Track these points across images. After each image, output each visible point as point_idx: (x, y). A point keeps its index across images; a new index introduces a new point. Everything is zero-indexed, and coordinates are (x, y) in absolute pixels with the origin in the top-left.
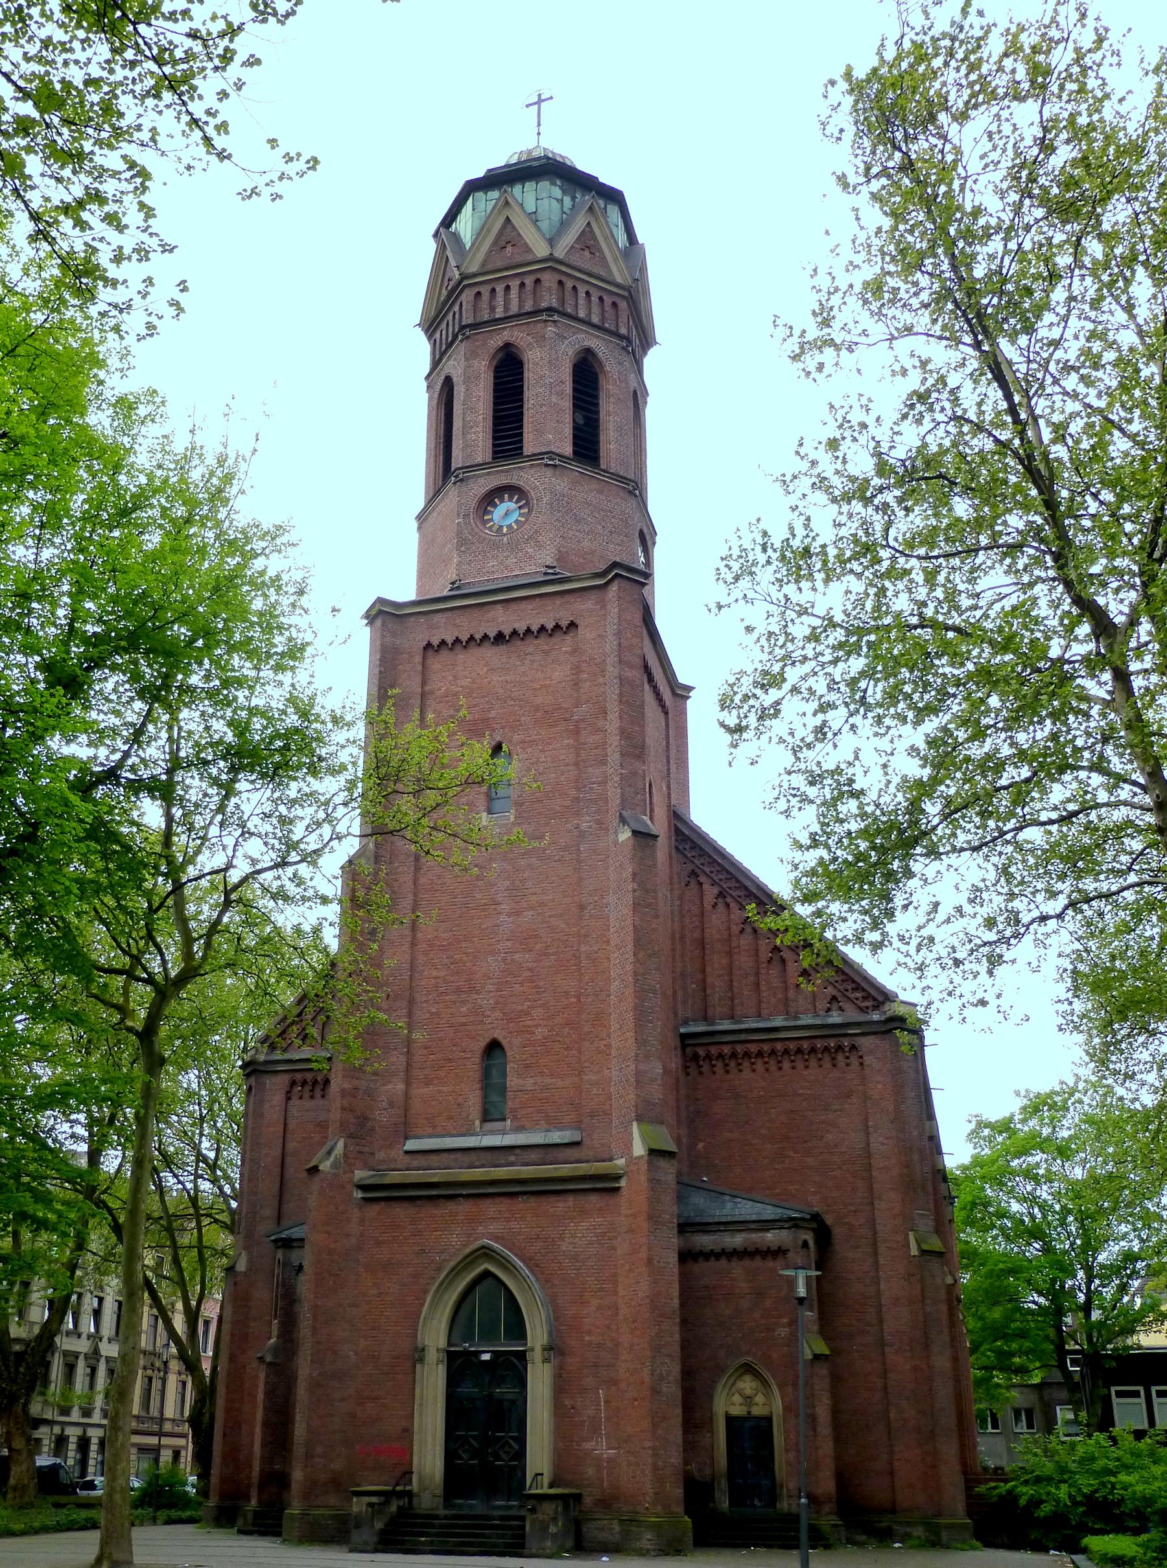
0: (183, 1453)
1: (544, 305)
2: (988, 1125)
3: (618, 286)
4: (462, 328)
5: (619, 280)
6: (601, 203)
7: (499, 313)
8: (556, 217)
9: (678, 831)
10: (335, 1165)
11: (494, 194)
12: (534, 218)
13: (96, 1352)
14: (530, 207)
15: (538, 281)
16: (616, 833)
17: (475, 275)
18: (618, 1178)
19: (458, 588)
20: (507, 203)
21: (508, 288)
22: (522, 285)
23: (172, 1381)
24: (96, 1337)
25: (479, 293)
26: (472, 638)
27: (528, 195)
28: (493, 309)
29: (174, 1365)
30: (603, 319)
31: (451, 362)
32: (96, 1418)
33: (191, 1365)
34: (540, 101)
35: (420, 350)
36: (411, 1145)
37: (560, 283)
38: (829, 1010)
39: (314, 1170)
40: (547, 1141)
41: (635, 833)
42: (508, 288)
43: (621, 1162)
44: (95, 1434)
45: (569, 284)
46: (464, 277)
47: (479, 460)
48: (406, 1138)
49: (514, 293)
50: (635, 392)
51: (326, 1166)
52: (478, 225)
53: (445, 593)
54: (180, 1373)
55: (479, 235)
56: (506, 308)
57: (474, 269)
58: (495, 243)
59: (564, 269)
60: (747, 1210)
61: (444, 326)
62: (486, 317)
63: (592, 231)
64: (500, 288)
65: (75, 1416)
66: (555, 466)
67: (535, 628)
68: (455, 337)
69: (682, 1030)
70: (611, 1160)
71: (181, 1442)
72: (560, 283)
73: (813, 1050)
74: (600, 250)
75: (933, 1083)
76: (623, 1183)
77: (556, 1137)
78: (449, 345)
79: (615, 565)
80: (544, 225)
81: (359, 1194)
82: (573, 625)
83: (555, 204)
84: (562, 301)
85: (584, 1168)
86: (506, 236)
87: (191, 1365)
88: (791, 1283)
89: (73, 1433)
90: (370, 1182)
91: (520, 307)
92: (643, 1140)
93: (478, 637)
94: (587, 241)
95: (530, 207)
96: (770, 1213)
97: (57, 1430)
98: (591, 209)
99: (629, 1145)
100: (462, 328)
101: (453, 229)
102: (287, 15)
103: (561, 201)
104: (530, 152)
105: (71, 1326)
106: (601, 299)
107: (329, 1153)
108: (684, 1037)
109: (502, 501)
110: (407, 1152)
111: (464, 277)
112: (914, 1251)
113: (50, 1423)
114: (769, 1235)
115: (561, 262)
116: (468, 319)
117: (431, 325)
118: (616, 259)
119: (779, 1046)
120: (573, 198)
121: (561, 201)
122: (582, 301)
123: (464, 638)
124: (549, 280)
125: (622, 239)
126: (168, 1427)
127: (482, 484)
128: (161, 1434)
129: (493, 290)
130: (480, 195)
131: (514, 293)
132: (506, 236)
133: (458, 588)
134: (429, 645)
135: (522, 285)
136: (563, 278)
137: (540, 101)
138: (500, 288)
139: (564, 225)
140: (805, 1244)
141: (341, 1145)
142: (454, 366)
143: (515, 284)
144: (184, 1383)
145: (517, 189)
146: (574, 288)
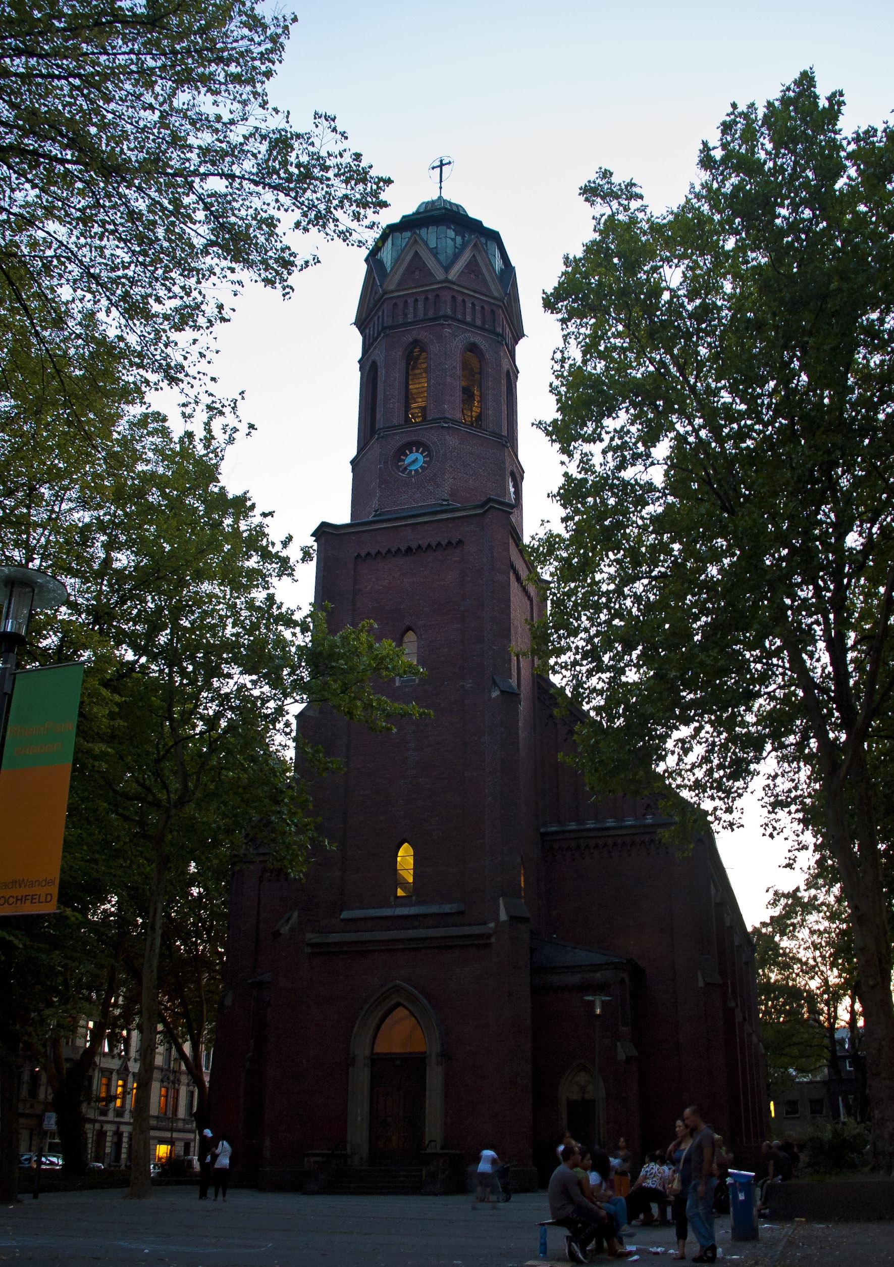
0: (192, 1144)
1: (441, 313)
2: (783, 895)
3: (495, 298)
4: (384, 328)
5: (496, 294)
6: (483, 240)
7: (410, 318)
8: (450, 251)
9: (540, 687)
10: (292, 930)
11: (407, 234)
12: (434, 252)
13: (126, 1069)
14: (432, 244)
15: (437, 296)
16: (490, 692)
17: (393, 291)
18: (489, 936)
19: (380, 515)
20: (416, 241)
21: (416, 300)
22: (426, 299)
23: (183, 1090)
24: (127, 1058)
25: (396, 304)
26: (389, 551)
27: (431, 235)
28: (405, 315)
29: (184, 1079)
30: (484, 322)
31: (376, 351)
32: (127, 1117)
33: (197, 1079)
34: (442, 165)
35: (355, 341)
36: (345, 915)
37: (453, 297)
38: (645, 815)
39: (277, 934)
40: (441, 911)
41: (502, 692)
42: (416, 300)
43: (492, 925)
44: (126, 1130)
45: (460, 298)
46: (385, 293)
47: (395, 422)
48: (342, 910)
49: (421, 305)
50: (508, 372)
51: (285, 930)
52: (395, 255)
53: (371, 518)
54: (188, 1085)
55: (397, 261)
56: (415, 315)
57: (391, 288)
58: (407, 269)
59: (455, 287)
60: (583, 956)
61: (371, 325)
62: (401, 321)
63: (476, 261)
64: (410, 301)
65: (111, 1116)
66: (448, 428)
67: (434, 544)
68: (379, 335)
69: (542, 830)
70: (485, 923)
71: (191, 1136)
72: (453, 297)
73: (633, 843)
74: (482, 274)
75: (725, 865)
76: (493, 940)
77: (447, 908)
78: (375, 339)
79: (490, 500)
80: (442, 257)
81: (308, 950)
82: (460, 542)
83: (450, 242)
84: (454, 311)
85: (466, 930)
86: (416, 267)
87: (197, 1079)
88: (591, 1004)
89: (109, 1128)
90: (314, 941)
91: (425, 314)
92: (507, 909)
93: (393, 550)
94: (472, 267)
95: (432, 244)
96: (598, 958)
97: (97, 1126)
98: (475, 245)
99: (497, 913)
100: (384, 328)
101: (378, 257)
102: (252, 135)
103: (454, 240)
104: (433, 202)
105: (107, 1050)
106: (483, 308)
107: (288, 921)
108: (543, 835)
109: (411, 452)
110: (343, 920)
111: (385, 293)
112: (701, 984)
113: (93, 1121)
114: (598, 975)
115: (453, 283)
116: (388, 321)
117: (361, 323)
118: (493, 280)
119: (610, 841)
120: (463, 237)
121: (454, 240)
122: (468, 310)
123: (384, 551)
124: (446, 296)
125: (498, 264)
126: (180, 1125)
127: (398, 441)
128: (172, 1130)
129: (406, 302)
130: (397, 234)
131: (421, 305)
132: (416, 267)
133: (380, 515)
134: (359, 556)
135: (426, 299)
136: (456, 295)
137: (442, 165)
138: (410, 301)
139: (456, 257)
140: (623, 980)
141: (296, 914)
142: (379, 356)
143: (421, 299)
144: (192, 1093)
145: (423, 232)
146: (464, 301)
